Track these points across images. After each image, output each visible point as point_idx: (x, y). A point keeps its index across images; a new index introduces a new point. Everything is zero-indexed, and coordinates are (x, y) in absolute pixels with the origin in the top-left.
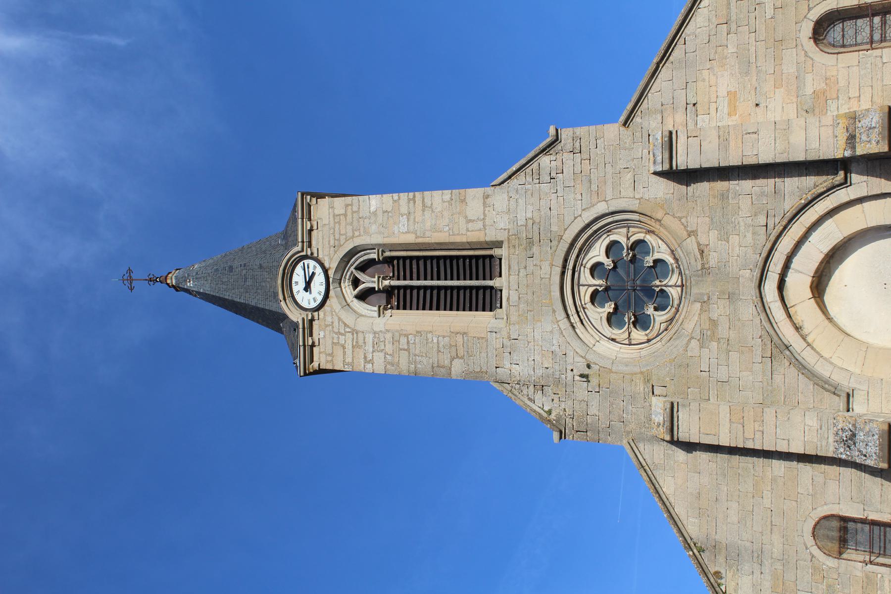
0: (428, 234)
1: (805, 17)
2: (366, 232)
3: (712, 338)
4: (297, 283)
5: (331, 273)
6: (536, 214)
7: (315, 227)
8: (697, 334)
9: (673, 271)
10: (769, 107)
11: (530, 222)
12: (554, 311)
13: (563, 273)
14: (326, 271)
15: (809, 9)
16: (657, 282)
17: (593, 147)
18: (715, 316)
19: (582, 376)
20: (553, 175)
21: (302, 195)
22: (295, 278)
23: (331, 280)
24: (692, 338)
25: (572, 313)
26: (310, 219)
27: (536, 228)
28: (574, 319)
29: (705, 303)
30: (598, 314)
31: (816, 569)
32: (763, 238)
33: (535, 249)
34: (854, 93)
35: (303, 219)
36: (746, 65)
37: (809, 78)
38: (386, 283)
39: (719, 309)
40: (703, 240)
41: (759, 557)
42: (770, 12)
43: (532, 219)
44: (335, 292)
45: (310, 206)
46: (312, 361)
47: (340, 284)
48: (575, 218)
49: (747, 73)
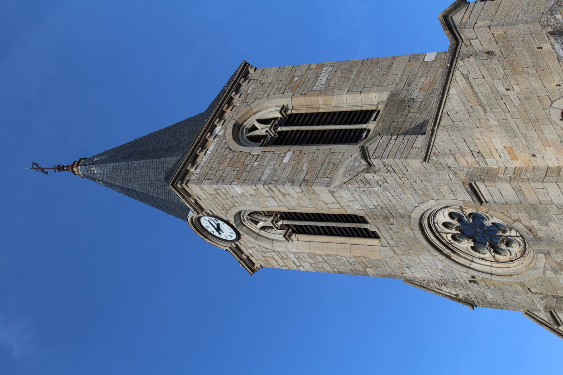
0: (296, 208)
1: (550, 106)
2: (244, 204)
4: (208, 227)
5: (232, 222)
6: (380, 203)
7: (198, 199)
8: (548, 267)
9: (247, 129)
10: (545, 157)
11: (379, 208)
12: (428, 251)
13: (477, 263)
14: (227, 222)
15: (552, 102)
16: (501, 234)
17: (405, 171)
18: (559, 261)
19: (470, 281)
20: (307, 154)
23: (235, 226)
24: (546, 270)
25: (445, 250)
26: (190, 196)
27: (386, 210)
28: (447, 251)
29: (547, 254)
30: (466, 245)
33: (392, 220)
35: (184, 198)
36: (511, 132)
40: (528, 224)
42: (516, 102)
43: (379, 205)
44: (243, 231)
45: (183, 189)
46: (253, 264)
47: (242, 224)
48: (415, 207)
49: (516, 136)
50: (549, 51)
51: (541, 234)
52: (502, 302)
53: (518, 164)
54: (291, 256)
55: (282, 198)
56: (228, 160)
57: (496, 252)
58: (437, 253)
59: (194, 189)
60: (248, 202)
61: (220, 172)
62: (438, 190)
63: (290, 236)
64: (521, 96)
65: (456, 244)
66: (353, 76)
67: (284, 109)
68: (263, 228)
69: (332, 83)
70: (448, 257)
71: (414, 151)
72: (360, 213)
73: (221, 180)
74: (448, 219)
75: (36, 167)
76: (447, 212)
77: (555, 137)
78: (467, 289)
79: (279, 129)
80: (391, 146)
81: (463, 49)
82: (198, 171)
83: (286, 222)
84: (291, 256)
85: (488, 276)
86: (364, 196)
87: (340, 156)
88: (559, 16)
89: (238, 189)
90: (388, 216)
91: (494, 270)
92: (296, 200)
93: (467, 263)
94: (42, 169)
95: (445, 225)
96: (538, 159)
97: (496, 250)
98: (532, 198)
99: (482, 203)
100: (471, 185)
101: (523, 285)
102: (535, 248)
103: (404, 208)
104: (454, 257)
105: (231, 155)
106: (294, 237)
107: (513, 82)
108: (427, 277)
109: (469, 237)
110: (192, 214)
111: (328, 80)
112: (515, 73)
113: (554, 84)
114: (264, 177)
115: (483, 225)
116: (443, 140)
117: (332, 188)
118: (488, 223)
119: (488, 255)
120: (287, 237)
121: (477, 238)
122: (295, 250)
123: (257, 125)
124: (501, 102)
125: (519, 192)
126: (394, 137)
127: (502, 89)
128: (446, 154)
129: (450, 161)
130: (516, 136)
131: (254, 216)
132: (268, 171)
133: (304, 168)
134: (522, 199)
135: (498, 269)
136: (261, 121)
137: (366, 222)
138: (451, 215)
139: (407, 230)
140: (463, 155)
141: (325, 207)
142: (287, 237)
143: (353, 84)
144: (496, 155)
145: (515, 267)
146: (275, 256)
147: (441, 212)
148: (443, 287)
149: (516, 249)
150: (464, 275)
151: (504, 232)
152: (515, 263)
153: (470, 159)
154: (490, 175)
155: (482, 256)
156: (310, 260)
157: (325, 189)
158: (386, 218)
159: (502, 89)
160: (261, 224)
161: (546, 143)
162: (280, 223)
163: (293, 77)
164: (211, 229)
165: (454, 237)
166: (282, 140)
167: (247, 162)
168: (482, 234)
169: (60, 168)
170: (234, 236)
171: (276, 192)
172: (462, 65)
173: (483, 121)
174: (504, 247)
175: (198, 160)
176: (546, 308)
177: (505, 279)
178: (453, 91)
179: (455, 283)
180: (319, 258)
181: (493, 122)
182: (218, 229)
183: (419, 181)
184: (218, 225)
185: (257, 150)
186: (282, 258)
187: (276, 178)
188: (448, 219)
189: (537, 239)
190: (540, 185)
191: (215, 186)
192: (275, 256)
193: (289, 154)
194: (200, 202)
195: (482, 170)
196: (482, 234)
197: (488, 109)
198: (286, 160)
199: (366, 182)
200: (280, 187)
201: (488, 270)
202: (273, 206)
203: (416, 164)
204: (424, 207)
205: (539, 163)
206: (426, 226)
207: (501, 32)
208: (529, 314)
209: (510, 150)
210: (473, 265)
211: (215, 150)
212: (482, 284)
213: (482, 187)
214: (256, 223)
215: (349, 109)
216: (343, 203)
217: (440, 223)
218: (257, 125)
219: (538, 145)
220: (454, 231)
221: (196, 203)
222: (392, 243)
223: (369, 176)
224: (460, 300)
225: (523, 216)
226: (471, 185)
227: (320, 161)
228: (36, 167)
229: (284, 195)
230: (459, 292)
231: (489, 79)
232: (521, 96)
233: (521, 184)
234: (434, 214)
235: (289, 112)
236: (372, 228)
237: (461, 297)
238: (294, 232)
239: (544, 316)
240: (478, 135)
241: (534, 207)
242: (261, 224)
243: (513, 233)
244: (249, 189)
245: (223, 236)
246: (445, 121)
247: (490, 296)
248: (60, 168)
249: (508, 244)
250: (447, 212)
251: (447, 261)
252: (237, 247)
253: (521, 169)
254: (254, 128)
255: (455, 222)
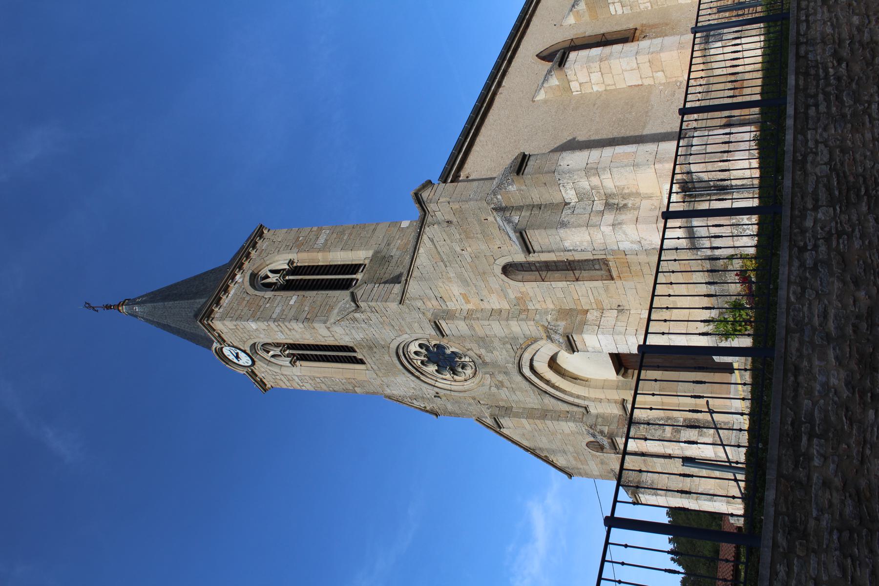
3: (503, 386)
5: (248, 352)
14: (245, 352)
21: (200, 321)
22: (226, 354)
25: (416, 372)
26: (214, 330)
28: (417, 374)
29: (492, 375)
31: (593, 455)
32: (513, 354)
33: (375, 350)
34: (540, 299)
36: (465, 282)
37: (510, 291)
38: (287, 352)
39: (501, 377)
40: (478, 352)
41: (564, 452)
46: (265, 385)
49: (468, 286)
50: (492, 222)
51: (488, 360)
52: (459, 412)
53: (470, 306)
54: (296, 378)
55: (288, 332)
56: (245, 302)
57: (454, 373)
58: (409, 375)
59: (218, 325)
60: (262, 336)
61: (239, 312)
62: (410, 327)
63: (295, 362)
64: (473, 255)
65: (424, 368)
66: (345, 238)
67: (291, 262)
68: (273, 356)
69: (329, 242)
70: (418, 378)
71: (392, 296)
72: (350, 344)
73: (240, 318)
74: (418, 349)
75: (88, 306)
76: (417, 343)
77: (497, 286)
78: (433, 403)
79: (287, 278)
80: (374, 292)
81: (429, 219)
82: (221, 310)
83: (291, 352)
84: (296, 378)
85: (448, 392)
86: (353, 331)
87: (335, 299)
88: (499, 197)
89: (253, 325)
90: (372, 346)
91: (453, 388)
92: (300, 333)
93: (433, 382)
94: (93, 308)
95: (416, 353)
96: (485, 303)
97: (455, 372)
98: (480, 332)
99: (443, 336)
100: (435, 322)
101: (474, 399)
102: (484, 370)
103: (385, 340)
104: (422, 378)
105: (247, 298)
106: (298, 363)
107: (466, 245)
108: (402, 393)
109: (434, 363)
110: (216, 345)
111: (326, 240)
112: (467, 238)
113: (496, 247)
114: (274, 316)
115: (444, 353)
116: (414, 287)
117: (328, 324)
118: (448, 352)
119: (448, 376)
120: (293, 363)
121: (440, 363)
122: (299, 374)
123: (270, 274)
124: (458, 260)
125: (471, 327)
126: (377, 285)
127: (458, 249)
128: (417, 299)
129: (419, 304)
130: (468, 286)
131: (266, 347)
132: (278, 310)
133: (306, 309)
134: (473, 333)
135: (456, 386)
136: (273, 271)
137: (355, 351)
138: (421, 346)
139: (387, 358)
140: (429, 299)
141: (323, 340)
142: (293, 363)
143: (346, 244)
144: (454, 300)
145: (468, 385)
146: (283, 378)
147: (412, 344)
148: (414, 401)
149: (469, 371)
150: (430, 392)
151: (460, 358)
152: (469, 382)
153: (435, 302)
154: (450, 315)
155: (444, 377)
156: (310, 381)
157: (323, 325)
158: (370, 348)
159: (458, 249)
160: (272, 353)
161: (491, 291)
162: (287, 352)
163: (299, 237)
164: (231, 357)
165: (422, 362)
166: (289, 286)
167: (261, 303)
168: (443, 359)
169: (108, 307)
170: (250, 363)
171: (284, 327)
172: (428, 231)
173: (444, 274)
174: (460, 370)
175: (221, 302)
176: (491, 415)
177: (461, 394)
178: (421, 250)
179: (423, 398)
180: (318, 380)
181: (452, 275)
182: (237, 357)
183: (396, 320)
184: (237, 354)
185: (269, 294)
186: (289, 380)
187: (284, 317)
188: (418, 349)
189: (485, 363)
190: (486, 323)
191: (235, 323)
192: (283, 378)
193: (294, 298)
194: (222, 335)
195: (444, 311)
196: (443, 359)
197: (448, 264)
198: (292, 302)
199: (355, 320)
200: (287, 324)
201: (449, 387)
202: (282, 338)
203: (393, 306)
204: (399, 340)
205: (486, 306)
206: (402, 354)
207: (458, 206)
208: (479, 420)
209: (464, 296)
210: (437, 384)
211: (235, 294)
212: (444, 398)
213: (443, 324)
214: (268, 352)
215: (342, 263)
216: (337, 336)
217: (412, 352)
218: (270, 274)
219: (485, 292)
220: (422, 358)
221: (219, 336)
222: (375, 367)
223: (357, 315)
224: (427, 411)
225: (474, 346)
226: (435, 322)
227: (318, 303)
228: (88, 306)
229: (290, 330)
230: (426, 405)
231: (448, 241)
232: (473, 255)
233: (473, 322)
234: (407, 345)
235: (295, 265)
236: (359, 356)
237: (428, 408)
238: (298, 359)
239: (490, 421)
240: (441, 284)
241: (482, 339)
242: (272, 353)
243: (467, 359)
244: (262, 325)
245: (241, 363)
246: (416, 273)
247: (450, 407)
248: (108, 307)
249: (463, 368)
250: (417, 343)
251: (418, 381)
252: (252, 371)
253: (473, 310)
254: (267, 277)
255: (423, 351)
